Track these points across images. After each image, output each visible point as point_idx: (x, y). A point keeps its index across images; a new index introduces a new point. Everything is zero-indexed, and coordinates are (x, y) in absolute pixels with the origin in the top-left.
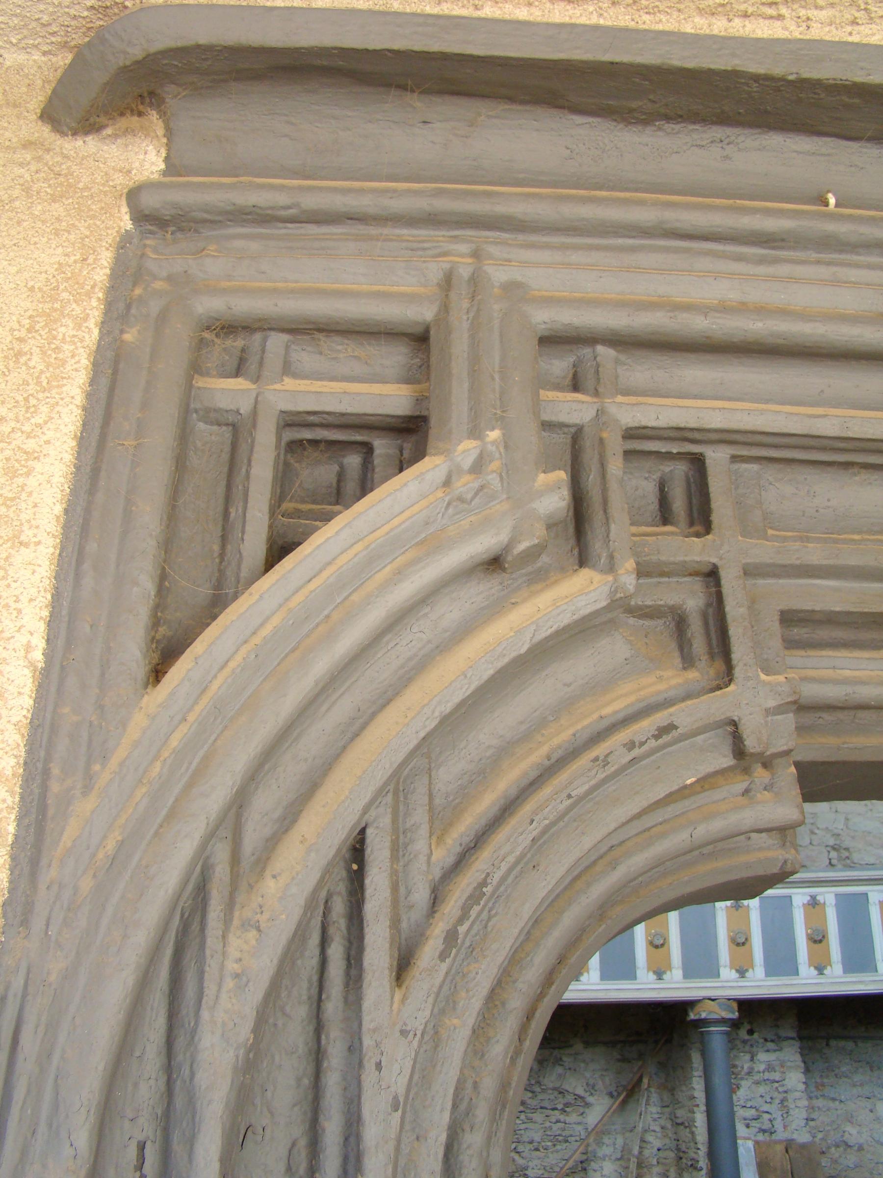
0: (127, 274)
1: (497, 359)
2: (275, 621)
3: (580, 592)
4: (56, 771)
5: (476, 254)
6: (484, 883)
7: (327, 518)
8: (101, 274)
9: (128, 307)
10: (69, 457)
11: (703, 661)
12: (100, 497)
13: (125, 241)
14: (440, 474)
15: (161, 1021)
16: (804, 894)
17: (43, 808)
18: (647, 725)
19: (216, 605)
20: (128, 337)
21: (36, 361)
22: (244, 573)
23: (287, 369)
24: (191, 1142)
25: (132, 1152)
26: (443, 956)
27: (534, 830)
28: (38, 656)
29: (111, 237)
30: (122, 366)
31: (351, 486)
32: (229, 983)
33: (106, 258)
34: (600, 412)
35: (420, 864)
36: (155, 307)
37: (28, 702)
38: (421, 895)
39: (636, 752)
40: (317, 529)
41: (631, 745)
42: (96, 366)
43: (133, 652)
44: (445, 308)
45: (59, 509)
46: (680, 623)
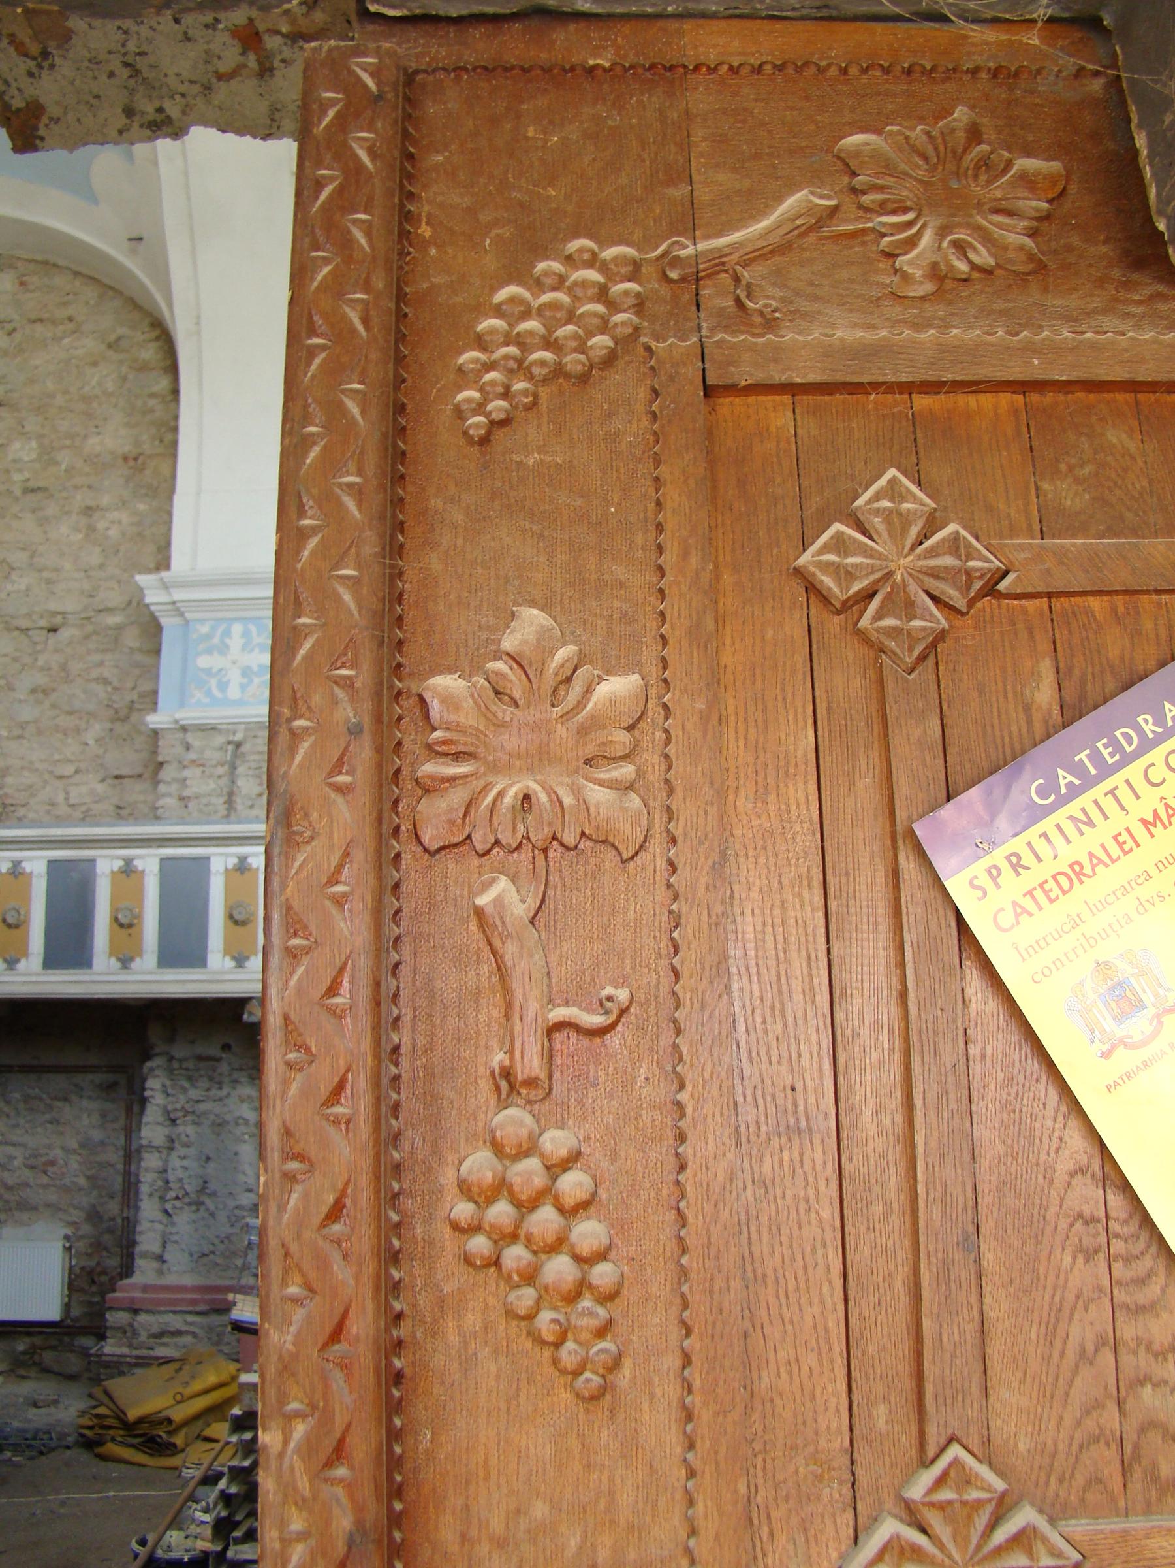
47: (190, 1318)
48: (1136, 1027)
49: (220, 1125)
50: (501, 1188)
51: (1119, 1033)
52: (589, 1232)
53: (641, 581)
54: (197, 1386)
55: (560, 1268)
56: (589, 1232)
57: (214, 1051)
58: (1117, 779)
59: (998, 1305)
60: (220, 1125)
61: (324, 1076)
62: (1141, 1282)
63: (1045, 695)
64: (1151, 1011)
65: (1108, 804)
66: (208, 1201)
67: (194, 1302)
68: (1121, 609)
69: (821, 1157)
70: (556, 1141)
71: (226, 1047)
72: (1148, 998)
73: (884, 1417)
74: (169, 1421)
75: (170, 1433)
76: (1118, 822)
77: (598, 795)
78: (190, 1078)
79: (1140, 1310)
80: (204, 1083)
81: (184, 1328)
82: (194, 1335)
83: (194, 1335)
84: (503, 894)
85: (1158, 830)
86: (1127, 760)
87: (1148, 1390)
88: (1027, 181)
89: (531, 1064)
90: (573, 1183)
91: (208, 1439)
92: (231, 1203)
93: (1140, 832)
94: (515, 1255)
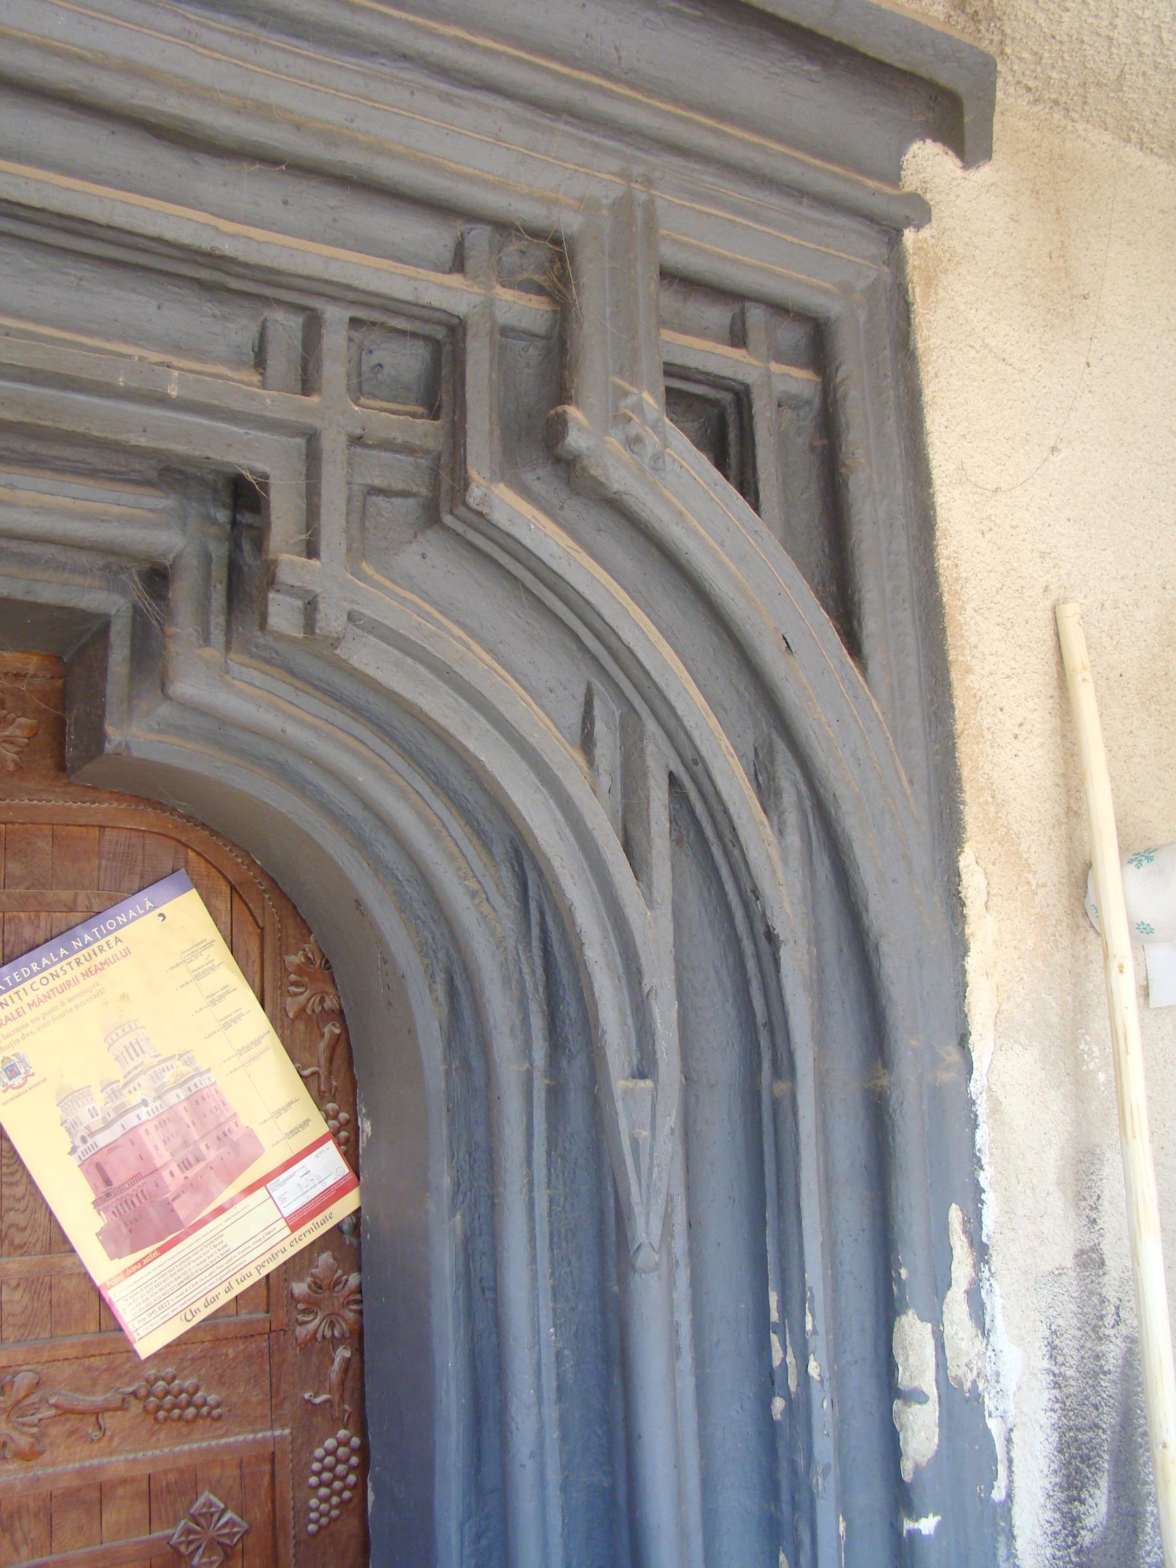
48: (17, 1081)
51: (10, 1083)
58: (19, 988)
62: (13, 1174)
64: (23, 1075)
65: (15, 997)
68: (33, 917)
72: (22, 1071)
76: (18, 1004)
79: (12, 1184)
85: (34, 1008)
86: (25, 980)
87: (12, 1213)
88: (20, 726)
93: (26, 1008)
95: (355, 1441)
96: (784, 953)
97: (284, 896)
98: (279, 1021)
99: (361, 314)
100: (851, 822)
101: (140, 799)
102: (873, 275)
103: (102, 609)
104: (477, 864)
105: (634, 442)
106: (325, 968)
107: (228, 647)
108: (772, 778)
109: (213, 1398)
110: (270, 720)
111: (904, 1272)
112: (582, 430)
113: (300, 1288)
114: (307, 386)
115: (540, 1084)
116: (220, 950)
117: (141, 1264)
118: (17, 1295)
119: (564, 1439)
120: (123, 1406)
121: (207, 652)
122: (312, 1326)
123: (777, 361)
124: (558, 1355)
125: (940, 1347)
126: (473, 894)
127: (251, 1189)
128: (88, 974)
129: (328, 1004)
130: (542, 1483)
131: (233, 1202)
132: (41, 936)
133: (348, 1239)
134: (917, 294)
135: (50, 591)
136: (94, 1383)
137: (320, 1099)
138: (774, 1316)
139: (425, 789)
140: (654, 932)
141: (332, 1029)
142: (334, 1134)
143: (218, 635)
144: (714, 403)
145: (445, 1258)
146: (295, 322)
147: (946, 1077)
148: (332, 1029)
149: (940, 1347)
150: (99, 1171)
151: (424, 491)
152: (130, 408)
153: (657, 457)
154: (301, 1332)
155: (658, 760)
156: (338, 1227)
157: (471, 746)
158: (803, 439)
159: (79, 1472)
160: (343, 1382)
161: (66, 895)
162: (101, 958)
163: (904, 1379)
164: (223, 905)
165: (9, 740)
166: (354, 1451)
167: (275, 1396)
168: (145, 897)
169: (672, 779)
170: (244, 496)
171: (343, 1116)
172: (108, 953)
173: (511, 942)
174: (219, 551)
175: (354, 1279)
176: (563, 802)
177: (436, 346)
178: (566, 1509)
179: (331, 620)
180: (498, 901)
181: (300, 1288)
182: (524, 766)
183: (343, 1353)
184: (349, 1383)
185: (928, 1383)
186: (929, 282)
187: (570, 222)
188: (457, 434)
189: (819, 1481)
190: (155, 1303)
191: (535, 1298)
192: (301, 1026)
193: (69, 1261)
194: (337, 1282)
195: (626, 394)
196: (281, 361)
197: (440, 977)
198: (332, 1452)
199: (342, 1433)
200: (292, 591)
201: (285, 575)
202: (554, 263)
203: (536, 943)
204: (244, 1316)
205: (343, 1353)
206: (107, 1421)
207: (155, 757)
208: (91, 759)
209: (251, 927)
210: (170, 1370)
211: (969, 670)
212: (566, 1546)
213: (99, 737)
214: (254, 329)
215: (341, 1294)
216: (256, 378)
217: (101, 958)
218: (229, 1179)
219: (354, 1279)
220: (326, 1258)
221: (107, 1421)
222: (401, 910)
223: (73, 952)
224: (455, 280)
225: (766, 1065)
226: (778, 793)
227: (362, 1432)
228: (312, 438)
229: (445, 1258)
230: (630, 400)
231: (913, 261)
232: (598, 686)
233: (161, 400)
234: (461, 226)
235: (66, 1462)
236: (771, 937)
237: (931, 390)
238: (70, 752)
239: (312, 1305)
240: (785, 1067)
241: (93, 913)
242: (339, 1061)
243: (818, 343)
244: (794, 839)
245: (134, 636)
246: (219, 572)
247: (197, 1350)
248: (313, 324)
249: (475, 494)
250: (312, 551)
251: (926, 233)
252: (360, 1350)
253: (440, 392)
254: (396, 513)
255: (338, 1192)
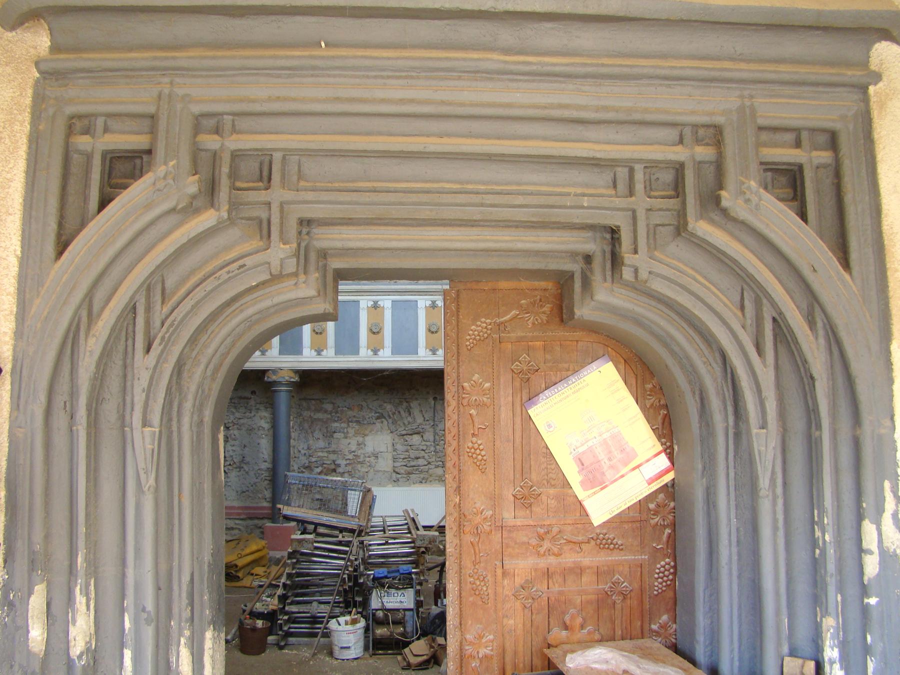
0: (39, 99)
1: (177, 129)
2: (95, 238)
3: (207, 219)
4: (27, 291)
5: (171, 83)
6: (175, 320)
7: (125, 187)
8: (28, 101)
9: (41, 113)
10: (23, 180)
11: (265, 240)
12: (35, 194)
13: (37, 82)
14: (152, 180)
15: (69, 366)
16: (426, 300)
17: (24, 302)
18: (236, 265)
19: (83, 225)
20: (41, 127)
21: (7, 141)
22: (90, 216)
23: (106, 130)
24: (77, 400)
25: (63, 403)
26: (160, 344)
27: (192, 302)
28: (19, 253)
29: (31, 82)
30: (40, 141)
31: (137, 172)
32: (88, 354)
33: (30, 92)
34: (223, 145)
35: (157, 314)
36: (51, 111)
37: (17, 269)
38: (158, 323)
39: (231, 275)
40: (121, 193)
41: (229, 272)
42: (30, 141)
43: (50, 249)
44: (158, 109)
45: (21, 200)
46: (261, 222)
47: (237, 522)
48: (551, 429)
49: (250, 430)
50: (473, 447)
52: (483, 453)
53: (490, 370)
54: (248, 551)
55: (480, 457)
56: (483, 453)
57: (247, 394)
59: (532, 463)
60: (250, 430)
61: (453, 434)
63: (543, 386)
66: (245, 467)
67: (239, 514)
69: (511, 444)
70: (479, 442)
71: (253, 393)
73: (518, 476)
74: (236, 566)
75: (236, 571)
77: (485, 399)
78: (235, 408)
80: (242, 410)
81: (235, 526)
82: (240, 530)
83: (240, 530)
84: (473, 412)
89: (476, 433)
90: (481, 447)
91: (252, 574)
92: (256, 468)
94: (474, 456)
95: (672, 564)
96: (817, 384)
97: (644, 363)
98: (644, 409)
99: (648, 165)
100: (843, 334)
101: (590, 331)
102: (856, 108)
103: (571, 269)
104: (706, 352)
105: (748, 201)
106: (660, 390)
107: (613, 282)
108: (813, 318)
109: (620, 542)
110: (628, 305)
111: (864, 505)
112: (727, 198)
113: (652, 506)
114: (631, 193)
115: (731, 432)
116: (621, 384)
117: (595, 493)
118: (553, 502)
119: (739, 560)
120: (588, 542)
121: (606, 285)
122: (656, 520)
123: (816, 149)
124: (738, 530)
125: (880, 534)
126: (705, 363)
127: (633, 469)
128: (574, 393)
129: (662, 403)
130: (730, 574)
131: (627, 473)
132: (558, 380)
133: (670, 489)
134: (875, 114)
135: (553, 266)
136: (579, 533)
137: (659, 438)
138: (816, 519)
139: (685, 326)
140: (767, 376)
141: (663, 412)
142: (665, 451)
143: (609, 278)
144: (791, 170)
145: (699, 495)
146: (626, 170)
147: (883, 431)
148: (663, 412)
149: (880, 534)
150: (580, 462)
151: (676, 223)
152: (573, 211)
153: (757, 205)
154: (653, 522)
155: (768, 315)
156: (666, 485)
157: (696, 313)
158: (828, 181)
159: (574, 562)
160: (668, 542)
161: (566, 366)
162: (579, 387)
163: (865, 545)
164: (622, 367)
165: (544, 313)
166: (672, 567)
167: (642, 544)
168: (594, 365)
169: (774, 319)
170: (614, 232)
171: (668, 444)
172: (581, 385)
173: (719, 380)
174: (608, 249)
175: (672, 504)
176: (731, 331)
177: (677, 170)
178: (739, 585)
179: (643, 275)
180: (714, 365)
181: (652, 506)
182: (716, 318)
183: (668, 531)
184: (670, 543)
185: (874, 547)
186: (882, 106)
187: (720, 120)
188: (684, 203)
189: (828, 579)
190: (602, 507)
191: (729, 508)
192: (651, 410)
193: (570, 491)
194: (666, 505)
195: (743, 183)
196: (622, 187)
197: (697, 393)
198: (664, 567)
199: (667, 560)
200: (629, 266)
201: (626, 261)
202: (715, 135)
203: (729, 380)
204: (631, 514)
205: (668, 531)
206: (583, 546)
207: (592, 319)
208: (571, 320)
209: (633, 375)
210: (605, 531)
211: (896, 271)
212: (739, 598)
213: (572, 313)
214: (612, 175)
215: (667, 509)
216: (614, 192)
217: (579, 387)
218: (626, 465)
219: (672, 504)
220: (661, 496)
221: (583, 546)
222: (682, 369)
223: (569, 385)
224: (679, 148)
225: (813, 425)
226: (815, 323)
227: (675, 560)
228: (634, 211)
229: (699, 495)
230: (746, 185)
231: (873, 100)
232: (745, 287)
233: (583, 207)
234: (680, 128)
235: (570, 558)
236: (812, 378)
237: (879, 156)
238: (564, 316)
239: (656, 513)
240: (819, 427)
241: (575, 372)
242: (666, 424)
243: (833, 141)
244: (822, 341)
245: (582, 278)
246: (608, 256)
247: (614, 525)
248: (631, 171)
249: (690, 227)
250: (636, 252)
251: (880, 85)
252: (674, 531)
253: (678, 188)
254: (666, 232)
255: (667, 471)
